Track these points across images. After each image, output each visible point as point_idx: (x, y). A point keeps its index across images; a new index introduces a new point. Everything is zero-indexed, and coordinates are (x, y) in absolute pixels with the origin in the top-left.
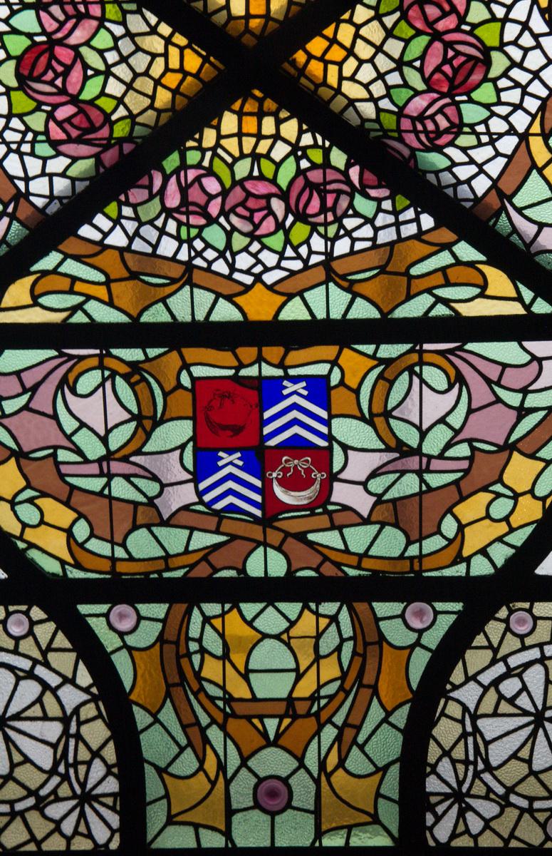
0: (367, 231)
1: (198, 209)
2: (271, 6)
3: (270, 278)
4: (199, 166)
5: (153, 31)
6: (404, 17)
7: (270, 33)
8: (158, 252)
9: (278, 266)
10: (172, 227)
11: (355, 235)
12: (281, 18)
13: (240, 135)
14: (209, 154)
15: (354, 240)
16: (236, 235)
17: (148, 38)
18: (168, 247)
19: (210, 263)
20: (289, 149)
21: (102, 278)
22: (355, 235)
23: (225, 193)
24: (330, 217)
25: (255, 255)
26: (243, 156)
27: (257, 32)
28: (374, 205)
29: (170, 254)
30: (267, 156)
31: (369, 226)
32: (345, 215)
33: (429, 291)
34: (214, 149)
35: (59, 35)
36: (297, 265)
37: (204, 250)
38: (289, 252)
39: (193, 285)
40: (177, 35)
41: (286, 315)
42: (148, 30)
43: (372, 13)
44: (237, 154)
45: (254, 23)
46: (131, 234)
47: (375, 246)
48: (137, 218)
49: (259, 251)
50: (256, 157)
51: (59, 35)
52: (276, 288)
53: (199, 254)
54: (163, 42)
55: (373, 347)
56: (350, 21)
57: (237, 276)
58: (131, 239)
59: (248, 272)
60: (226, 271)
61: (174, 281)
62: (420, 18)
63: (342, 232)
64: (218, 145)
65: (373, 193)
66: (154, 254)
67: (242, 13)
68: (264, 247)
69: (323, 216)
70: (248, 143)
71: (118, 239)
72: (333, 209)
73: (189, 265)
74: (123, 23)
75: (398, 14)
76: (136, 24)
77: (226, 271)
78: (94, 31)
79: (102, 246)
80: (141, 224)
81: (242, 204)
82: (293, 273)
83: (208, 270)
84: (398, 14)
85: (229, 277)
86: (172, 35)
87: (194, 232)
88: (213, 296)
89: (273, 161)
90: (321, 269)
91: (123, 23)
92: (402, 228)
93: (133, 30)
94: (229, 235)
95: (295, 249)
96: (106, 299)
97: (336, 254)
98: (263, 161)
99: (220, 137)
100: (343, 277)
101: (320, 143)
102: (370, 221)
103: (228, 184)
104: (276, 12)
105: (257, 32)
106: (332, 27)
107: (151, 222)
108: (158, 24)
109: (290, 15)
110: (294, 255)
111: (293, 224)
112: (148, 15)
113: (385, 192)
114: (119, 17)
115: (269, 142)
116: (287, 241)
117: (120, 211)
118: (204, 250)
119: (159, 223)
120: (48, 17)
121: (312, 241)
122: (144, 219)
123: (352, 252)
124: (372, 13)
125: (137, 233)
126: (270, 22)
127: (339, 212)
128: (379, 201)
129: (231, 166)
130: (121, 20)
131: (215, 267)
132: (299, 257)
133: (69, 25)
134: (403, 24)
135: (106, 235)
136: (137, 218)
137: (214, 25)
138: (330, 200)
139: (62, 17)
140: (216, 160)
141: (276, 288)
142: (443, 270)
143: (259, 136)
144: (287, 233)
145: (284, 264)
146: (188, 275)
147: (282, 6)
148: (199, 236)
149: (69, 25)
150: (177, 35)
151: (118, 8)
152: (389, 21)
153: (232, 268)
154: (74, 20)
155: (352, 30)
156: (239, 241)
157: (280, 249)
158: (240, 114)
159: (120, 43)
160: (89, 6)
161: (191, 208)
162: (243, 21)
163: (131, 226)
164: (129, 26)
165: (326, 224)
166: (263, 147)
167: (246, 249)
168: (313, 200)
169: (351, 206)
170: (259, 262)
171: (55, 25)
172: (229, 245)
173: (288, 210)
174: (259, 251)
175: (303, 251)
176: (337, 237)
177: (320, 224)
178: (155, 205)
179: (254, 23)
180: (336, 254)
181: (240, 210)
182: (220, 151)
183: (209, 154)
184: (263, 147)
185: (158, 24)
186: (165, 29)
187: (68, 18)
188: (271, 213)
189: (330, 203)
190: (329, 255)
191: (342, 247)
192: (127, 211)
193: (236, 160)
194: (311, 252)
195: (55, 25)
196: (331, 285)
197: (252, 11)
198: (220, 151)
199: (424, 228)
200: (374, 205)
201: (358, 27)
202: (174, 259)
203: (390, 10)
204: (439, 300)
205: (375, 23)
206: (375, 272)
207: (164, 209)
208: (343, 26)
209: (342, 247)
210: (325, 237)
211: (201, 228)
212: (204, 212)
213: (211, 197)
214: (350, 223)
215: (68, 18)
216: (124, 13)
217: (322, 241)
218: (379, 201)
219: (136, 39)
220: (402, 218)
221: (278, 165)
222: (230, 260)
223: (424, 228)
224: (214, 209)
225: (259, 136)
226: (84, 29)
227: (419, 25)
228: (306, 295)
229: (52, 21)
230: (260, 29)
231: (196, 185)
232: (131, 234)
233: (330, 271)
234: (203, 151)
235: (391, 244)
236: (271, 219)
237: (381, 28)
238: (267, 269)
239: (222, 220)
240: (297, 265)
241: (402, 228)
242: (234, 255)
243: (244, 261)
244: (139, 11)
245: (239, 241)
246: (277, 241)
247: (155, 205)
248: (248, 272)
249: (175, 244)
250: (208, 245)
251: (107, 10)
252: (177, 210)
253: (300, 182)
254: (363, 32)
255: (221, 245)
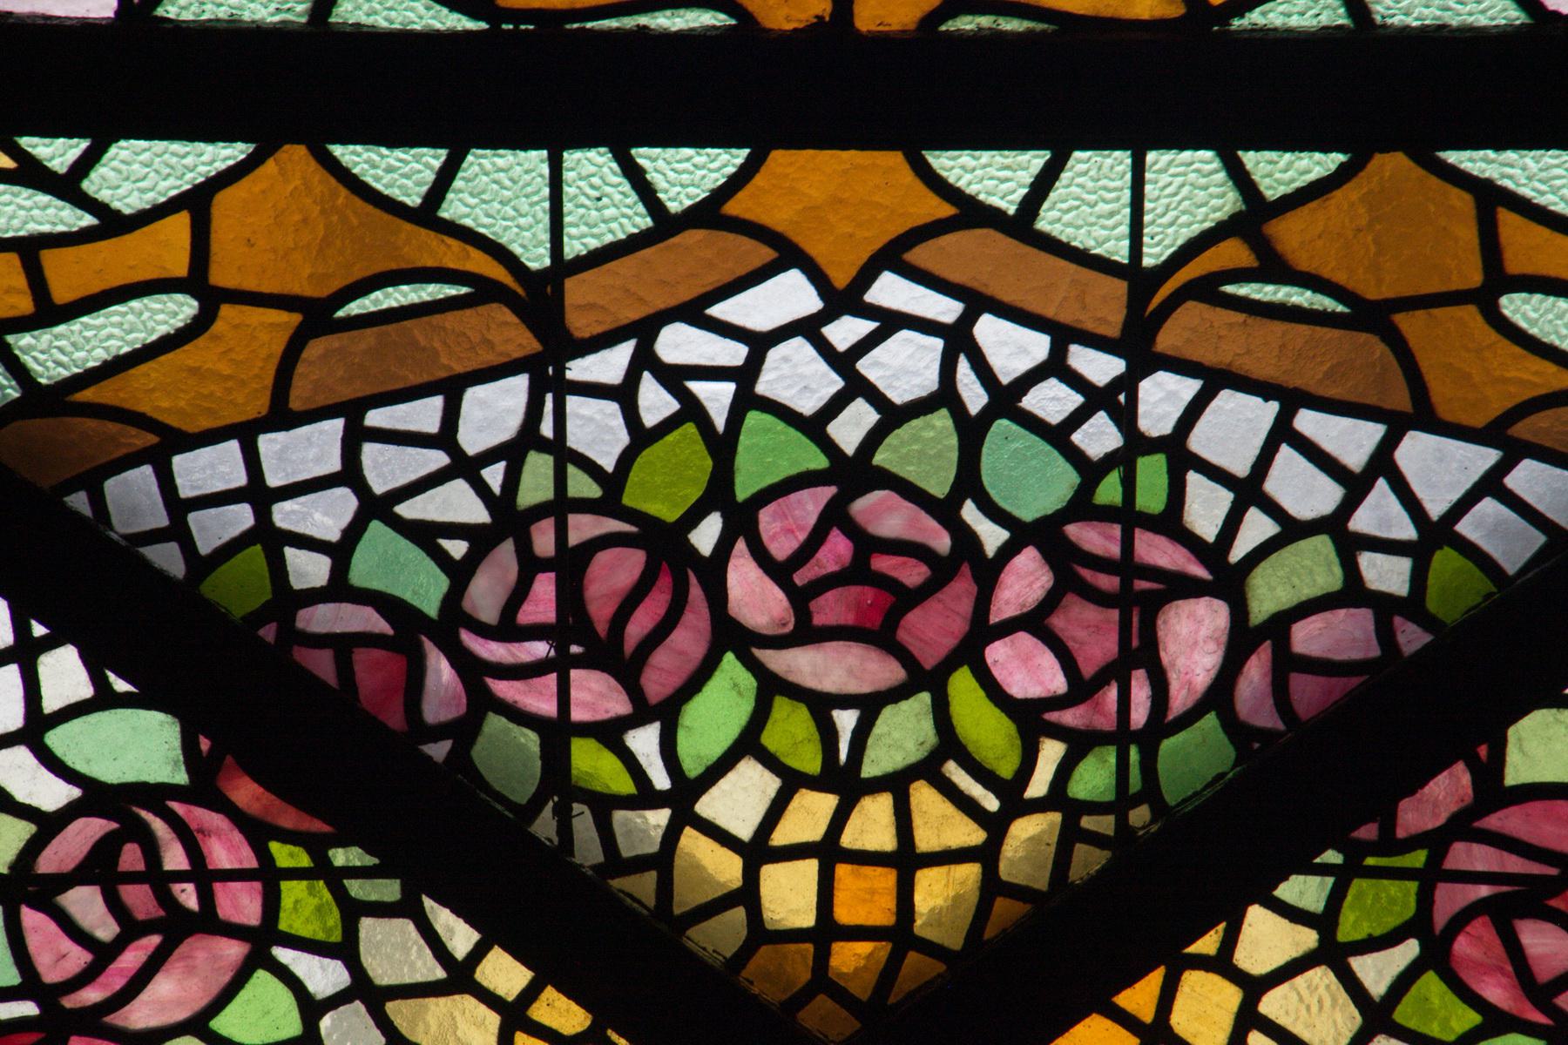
0: (385, 468)
1: (1086, 574)
2: (918, 898)
3: (791, 295)
4: (1080, 745)
5: (460, 978)
6: (1437, 958)
7: (910, 995)
8: (1274, 407)
9: (760, 343)
10: (1206, 508)
11: (437, 459)
12: (955, 941)
13: (906, 860)
14: (1038, 787)
15: (445, 438)
16: (939, 484)
17: (438, 1007)
18: (1235, 427)
19: (1055, 367)
20: (709, 806)
21: (1520, 308)
22: (437, 459)
23: (970, 651)
24: (544, 540)
25: (857, 387)
26: (897, 784)
27: (861, 990)
28: (363, 572)
29: (1228, 401)
30: (792, 782)
31: (379, 487)
32: (481, 540)
33: (112, 223)
34: (1016, 804)
35: (91, 995)
36: (680, 344)
37: (1077, 418)
38: (716, 397)
39: (1134, 274)
40: (550, 993)
41: (724, 161)
42: (440, 974)
43: (1308, 939)
44: (923, 796)
45: (849, 957)
46: (1382, 484)
47: (352, 411)
48: (1350, 546)
49: (835, 406)
50: (846, 782)
51: (91, 995)
52: (766, 254)
53: (1096, 399)
54: (493, 1020)
55: (424, 162)
56: (1222, 964)
57: (946, 309)
58: (1383, 463)
59: (891, 322)
60: (990, 331)
61: (1207, 290)
62: (1501, 970)
63: (494, 476)
64: (996, 826)
65: (367, 620)
66: (1292, 400)
67: (807, 920)
68: (814, 427)
69: (574, 539)
70: (872, 826)
71: (1439, 466)
72: (530, 566)
73: (1142, 356)
74: (346, 950)
75: (1409, 950)
76: (394, 952)
77: (990, 331)
78: (226, 978)
79: (1506, 436)
80: (1334, 525)
81: (908, 599)
82: (694, 313)
83: (1063, 335)
84: (1409, 950)
85: (977, 303)
86: (530, 994)
87: (1109, 491)
88: (1049, 221)
89: (771, 762)
90: (581, 324)
91: (346, 950)
92: (238, 477)
93: (382, 972)
94: (969, 482)
95: (692, 410)
96: (1508, 221)
97: (519, 385)
98: (809, 761)
99: (987, 855)
100: (484, 292)
101: (583, 822)
102: (376, 508)
103: (962, 684)
104: (936, 916)
105: (861, 990)
106: (1153, 982)
107: (1292, 530)
108: (478, 954)
109: (989, 933)
110: (697, 387)
111: (694, 516)
112: (444, 919)
113: (323, 618)
114: (329, 926)
115: (782, 836)
116: (722, 446)
117: (1419, 578)
118: (1077, 418)
119: (1257, 528)
120: (52, 927)
121: (622, 438)
122: (1322, 545)
123: (452, 390)
124: (1308, 939)
125: (1355, 486)
126: (913, 957)
127: (506, 552)
128: (339, 589)
129: (949, 744)
130: (336, 937)
131: (1038, 346)
132: (674, 378)
133: (132, 958)
134: (1431, 985)
135: (1491, 485)
136: (1350, 546)
137: (693, 962)
138: (542, 603)
139: (105, 929)
140: (1006, 769)
141: (766, 254)
142: (48, 313)
143: (828, 852)
144: (718, 494)
145: (733, 353)
146: (1147, 307)
147: (957, 899)
148: (1090, 471)
149: (132, 958)
150: (550, 993)
151: (327, 895)
152: (1376, 972)
153: (958, 341)
154: (155, 940)
155: (1230, 996)
156: (925, 452)
157: (754, 418)
158: (900, 933)
159: (326, 1023)
160: (218, 887)
161: (1108, 582)
162: (809, 948)
163: (1380, 514)
164: (369, 961)
165: (561, 506)
166: (809, 816)
167: (893, 416)
168: (628, 583)
169: (460, 574)
170: (843, 362)
171: (78, 958)
172: (972, 432)
173: (714, 570)
174: (835, 406)
175: (655, 402)
176: (513, 453)
177: (584, 506)
178: (1270, 592)
179: (849, 957)
180: (519, 385)
181: (913, 574)
182: (991, 803)
183: (1038, 787)
184: (809, 816)
185: (478, 954)
186: (505, 973)
187: (131, 929)
188: (778, 571)
189: (545, 586)
190: (549, 383)
191: (493, 411)
192: (1386, 574)
193: (928, 769)
194: (624, 394)
195: (78, 958)
196: (537, 257)
197: (845, 913)
198: (991, 803)
199: (144, 475)
200: (363, 572)
201: (1254, 987)
202: (1215, 380)
203: (1378, 932)
204: (67, 187)
205: (1321, 977)
206: (355, 308)
207: (1227, 579)
208: (1193, 980)
209: (493, 411)
210: (564, 456)
211: (1081, 506)
212: (1066, 562)
213: (1035, 622)
214: (458, 504)
215: (131, 929)
216: (352, 911)
217: (576, 439)
218: (339, 589)
219: (391, 1007)
220: (241, 517)
221: (749, 744)
222: (964, 368)
223: (144, 475)
224: (1025, 582)
225: (828, 852)
226: (191, 970)
227: (1497, 992)
228: (643, 221)
229: (67, 945)
230: (871, 979)
231: (1088, 670)
232: (1382, 484)
233: (540, 311)
234: (1057, 797)
235: (282, 417)
236: (781, 549)
237: (1343, 997)
238: (809, 328)
239: (992, 536)
240: (680, 344)
241: (238, 477)
242: (946, 396)
243: (905, 366)
244: (408, 909)
245: (925, 452)
246: (766, 454)
247: (1270, 592)
248: (891, 322)
249: (1200, 442)
250: (1059, 436)
251: (287, 902)
252: (1181, 587)
253: (659, 679)
254: (1272, 1005)
255: (1005, 447)
